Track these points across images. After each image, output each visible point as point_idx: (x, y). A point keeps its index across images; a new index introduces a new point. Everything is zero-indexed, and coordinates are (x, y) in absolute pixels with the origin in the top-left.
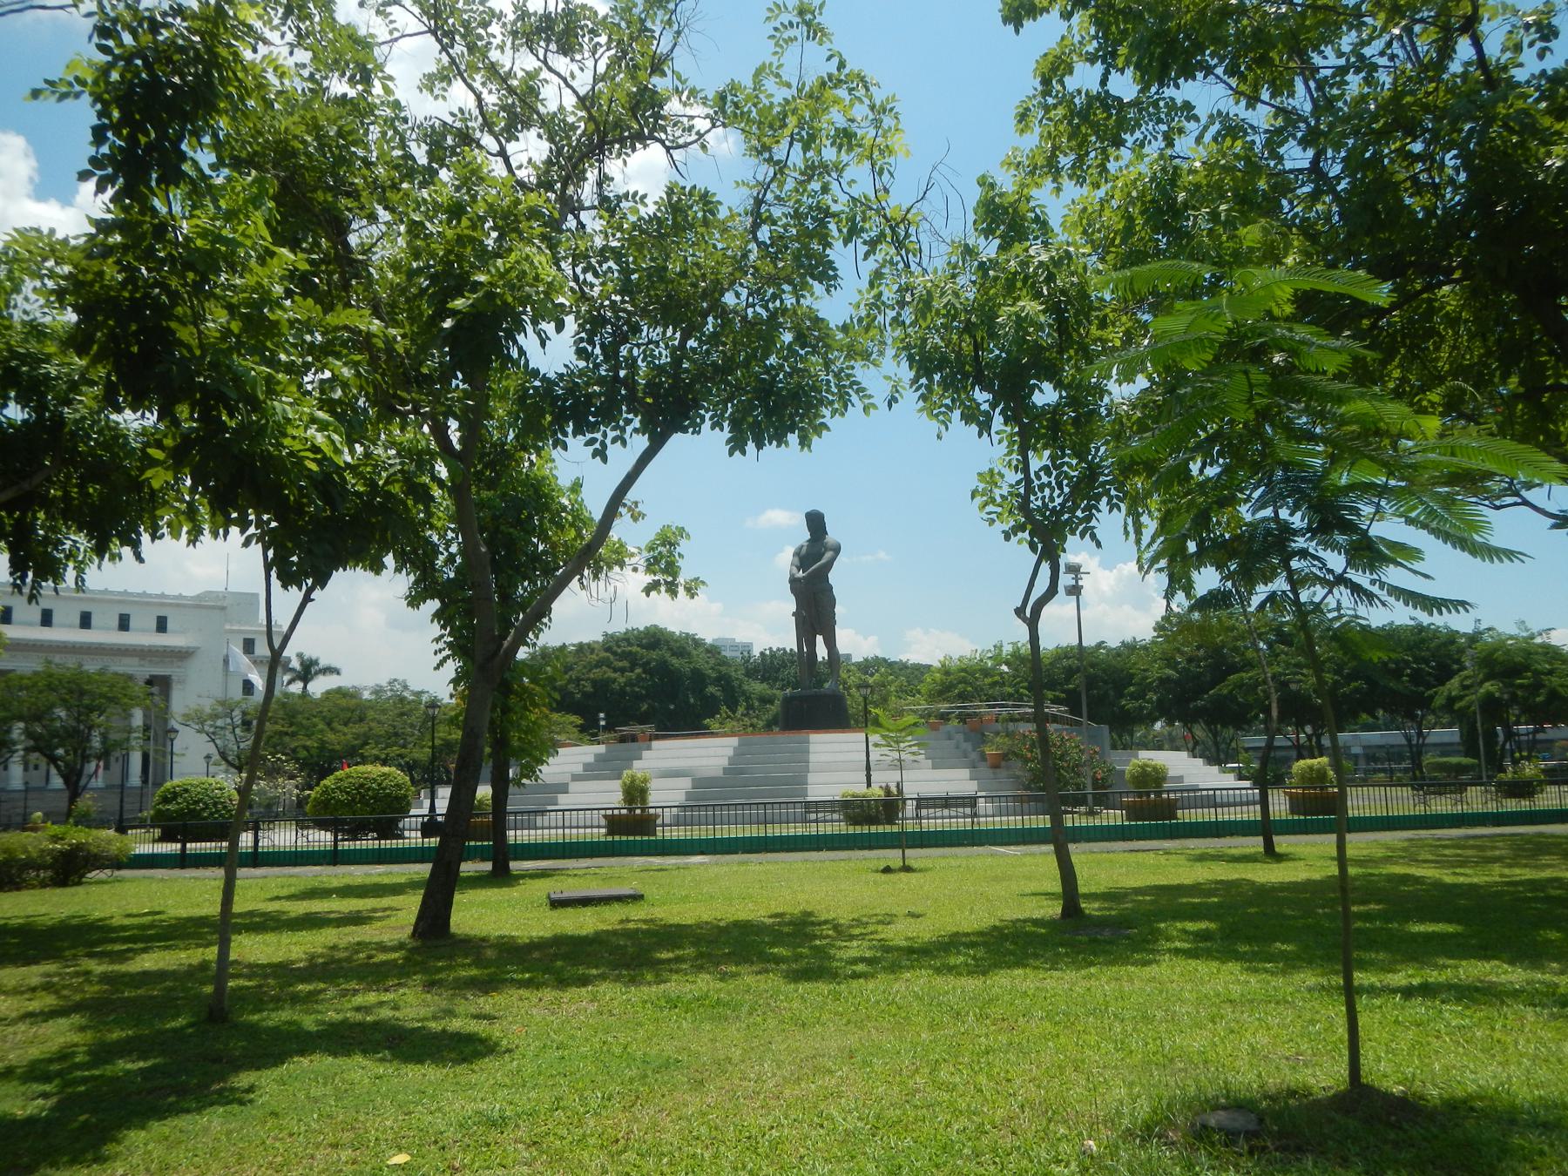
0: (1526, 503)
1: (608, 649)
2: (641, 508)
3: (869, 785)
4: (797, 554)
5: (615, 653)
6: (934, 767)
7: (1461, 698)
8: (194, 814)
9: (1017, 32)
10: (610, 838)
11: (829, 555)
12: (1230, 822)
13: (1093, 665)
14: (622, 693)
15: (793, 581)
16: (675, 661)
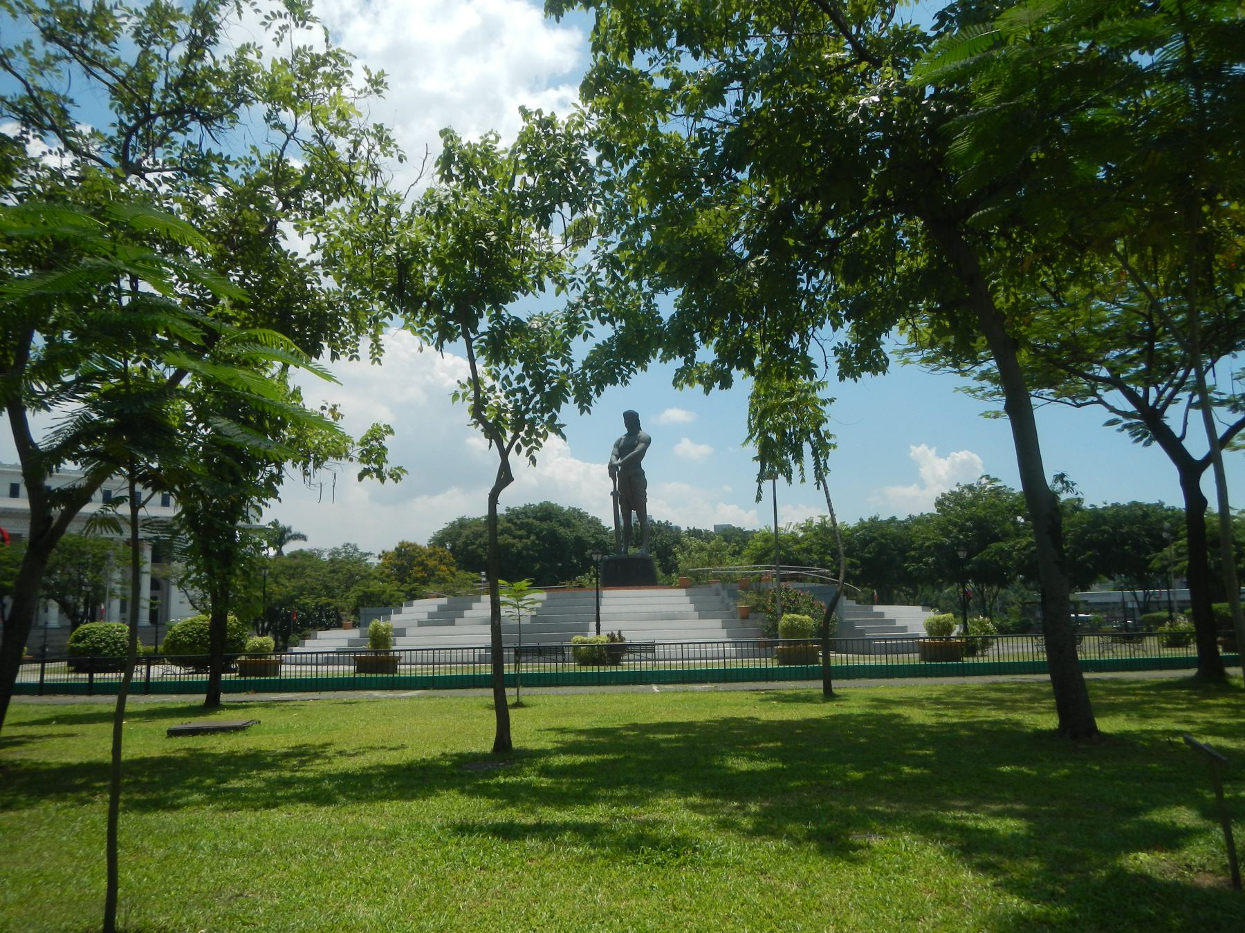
0: (1100, 401)
1: (510, 521)
2: (339, 410)
3: (598, 633)
4: (617, 445)
5: (515, 524)
6: (701, 617)
7: (1176, 563)
8: (97, 650)
9: (558, 20)
10: (357, 676)
11: (641, 446)
12: (859, 666)
13: (883, 536)
14: (519, 554)
15: (612, 468)
16: (561, 530)
